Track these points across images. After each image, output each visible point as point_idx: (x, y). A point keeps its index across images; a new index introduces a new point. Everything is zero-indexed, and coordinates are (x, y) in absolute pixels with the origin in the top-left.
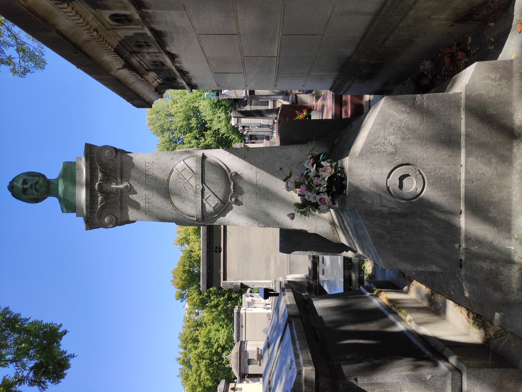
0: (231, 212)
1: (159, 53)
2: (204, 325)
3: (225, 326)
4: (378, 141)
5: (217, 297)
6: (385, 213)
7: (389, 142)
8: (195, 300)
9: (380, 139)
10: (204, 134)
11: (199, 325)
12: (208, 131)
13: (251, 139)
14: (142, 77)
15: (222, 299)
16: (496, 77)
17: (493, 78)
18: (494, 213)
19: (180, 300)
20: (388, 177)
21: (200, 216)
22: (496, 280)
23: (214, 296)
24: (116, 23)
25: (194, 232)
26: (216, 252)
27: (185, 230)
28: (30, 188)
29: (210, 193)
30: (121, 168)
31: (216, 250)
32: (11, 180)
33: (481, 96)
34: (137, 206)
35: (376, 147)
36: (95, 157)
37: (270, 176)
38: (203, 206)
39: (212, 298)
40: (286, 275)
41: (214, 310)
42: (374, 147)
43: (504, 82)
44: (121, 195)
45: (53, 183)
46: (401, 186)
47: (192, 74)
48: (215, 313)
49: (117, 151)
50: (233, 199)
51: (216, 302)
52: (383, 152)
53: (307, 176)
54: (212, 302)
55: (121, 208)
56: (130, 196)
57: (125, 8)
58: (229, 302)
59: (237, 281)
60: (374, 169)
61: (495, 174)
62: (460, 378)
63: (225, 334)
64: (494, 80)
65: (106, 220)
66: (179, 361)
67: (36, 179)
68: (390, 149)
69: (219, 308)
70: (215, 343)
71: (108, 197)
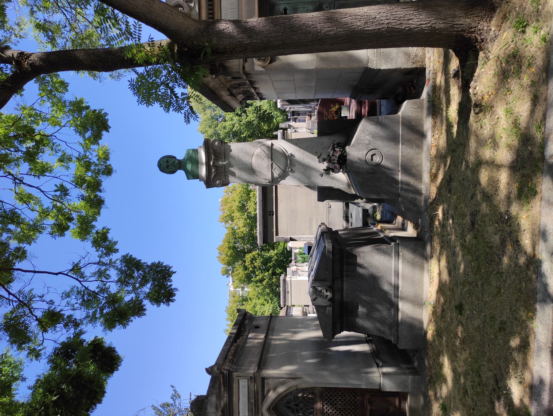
0: (288, 177)
2: (249, 300)
3: (270, 301)
4: (361, 138)
5: (262, 272)
8: (240, 275)
10: (246, 110)
11: (245, 300)
12: (250, 107)
13: (293, 115)
14: (235, 98)
15: (266, 274)
18: (414, 171)
19: (226, 276)
20: (366, 155)
21: (271, 180)
23: (259, 271)
25: (238, 210)
26: (270, 215)
27: (229, 207)
29: (276, 166)
33: (409, 116)
34: (234, 174)
37: (311, 155)
38: (272, 174)
39: (257, 273)
41: (259, 285)
43: (419, 109)
46: (372, 159)
47: (342, 214)
48: (260, 287)
50: (290, 169)
51: (261, 276)
53: (329, 155)
54: (257, 277)
55: (225, 176)
56: (230, 169)
58: (274, 277)
63: (271, 308)
64: (415, 109)
65: (218, 182)
66: (226, 333)
67: (174, 160)
69: (264, 283)
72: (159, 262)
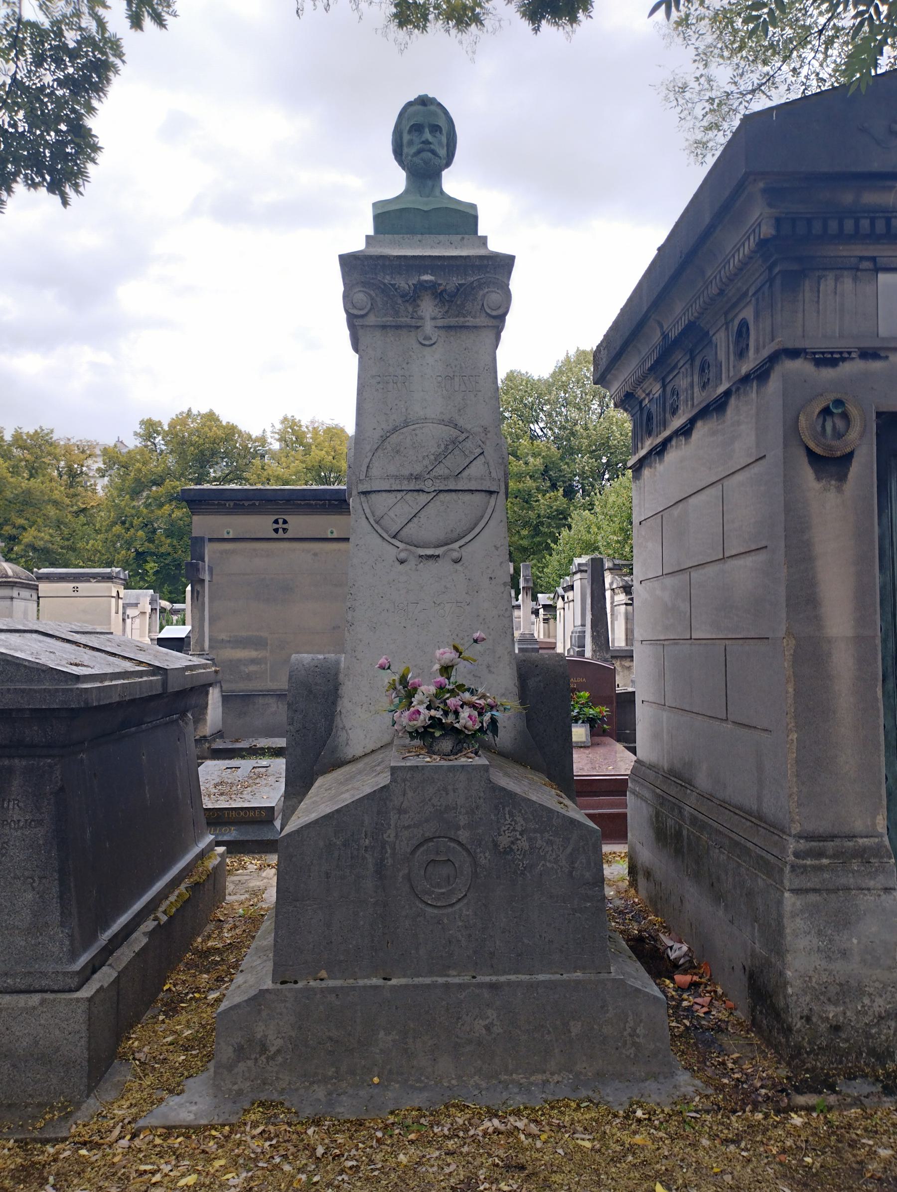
1: (693, 405)
6: (385, 836)
7: (518, 839)
9: (523, 822)
16: (638, 1037)
17: (638, 1031)
22: (258, 1050)
24: (736, 329)
26: (276, 522)
28: (423, 139)
30: (467, 327)
31: (281, 521)
32: (439, 100)
35: (507, 816)
36: (487, 275)
40: (221, 687)
42: (507, 812)
44: (411, 326)
45: (433, 186)
49: (500, 320)
52: (499, 829)
57: (757, 350)
59: (207, 572)
60: (467, 813)
61: (459, 1041)
62: (67, 987)
67: (442, 152)
68: (505, 842)
70: (27, 519)
71: (407, 301)
72: (100, 148)
